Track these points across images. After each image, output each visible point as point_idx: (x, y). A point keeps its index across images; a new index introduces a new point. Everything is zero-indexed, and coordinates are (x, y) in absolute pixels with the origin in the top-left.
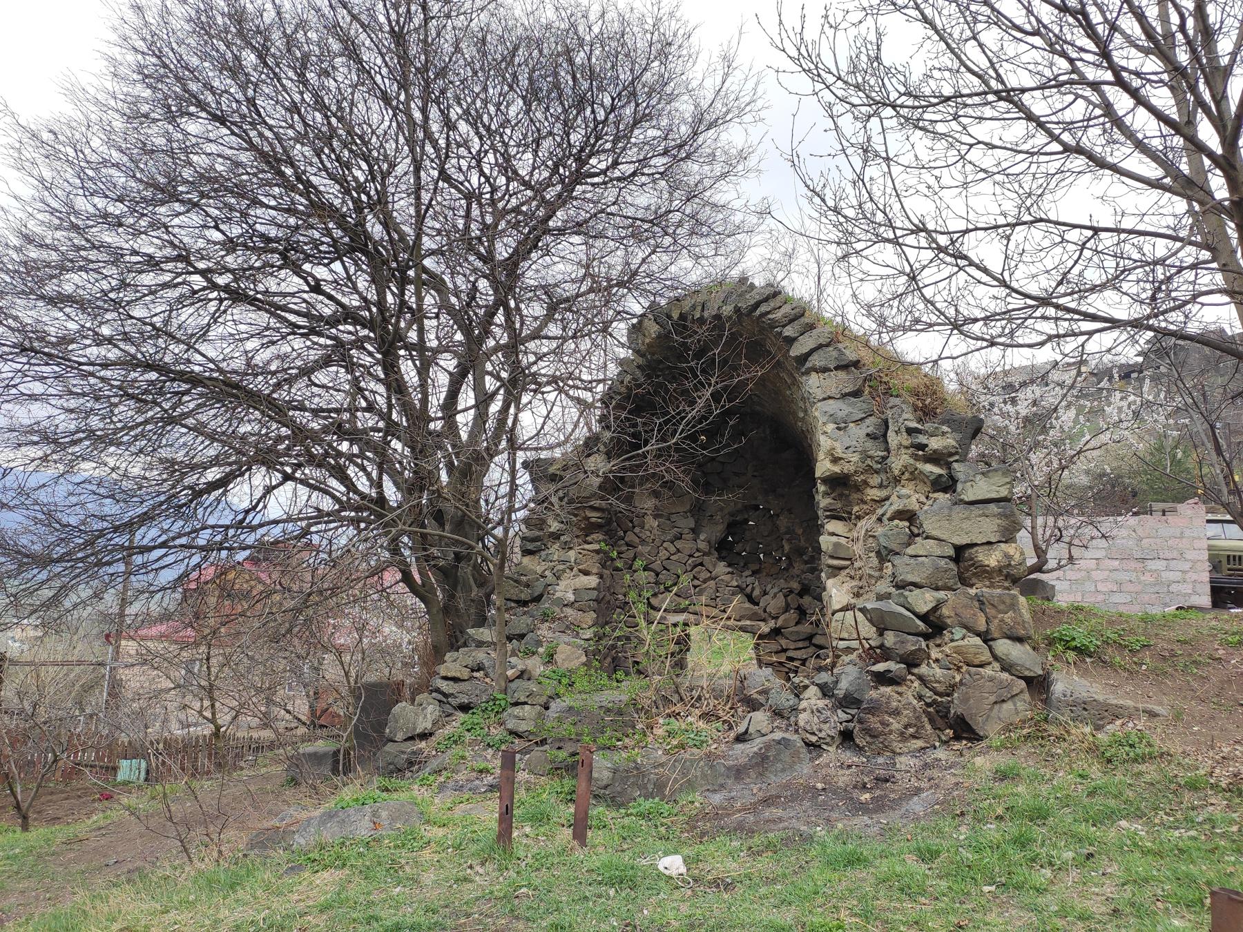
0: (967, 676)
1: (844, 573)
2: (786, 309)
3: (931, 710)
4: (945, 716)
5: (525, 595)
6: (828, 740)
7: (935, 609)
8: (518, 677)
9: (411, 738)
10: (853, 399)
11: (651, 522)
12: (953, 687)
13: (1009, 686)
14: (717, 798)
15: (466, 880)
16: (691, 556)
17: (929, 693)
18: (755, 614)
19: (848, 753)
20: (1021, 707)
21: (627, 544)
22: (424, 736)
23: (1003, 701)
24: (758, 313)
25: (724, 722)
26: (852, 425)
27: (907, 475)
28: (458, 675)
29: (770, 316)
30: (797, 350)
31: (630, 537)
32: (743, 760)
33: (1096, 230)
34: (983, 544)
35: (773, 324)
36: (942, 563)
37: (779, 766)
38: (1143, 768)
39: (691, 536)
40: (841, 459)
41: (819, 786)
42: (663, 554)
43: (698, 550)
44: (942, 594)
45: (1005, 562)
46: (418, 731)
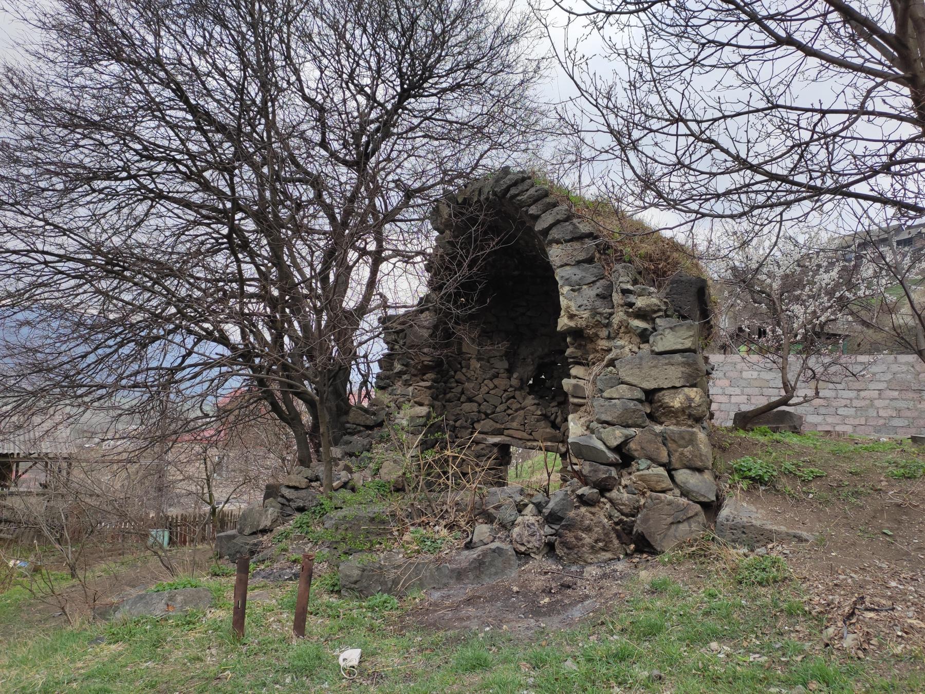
0: (649, 500)
1: (583, 409)
2: (532, 191)
3: (618, 527)
4: (631, 532)
5: (371, 420)
6: (535, 550)
7: (626, 442)
8: (341, 487)
9: (254, 533)
10: (586, 265)
11: (475, 364)
12: (638, 509)
13: (685, 509)
14: (436, 595)
15: (199, 659)
16: (505, 391)
17: (617, 514)
18: (555, 437)
19: (550, 561)
20: (693, 529)
21: (457, 382)
22: (264, 531)
23: (679, 522)
24: (508, 195)
25: (465, 531)
26: (585, 287)
27: (623, 329)
28: (297, 484)
29: (519, 198)
30: (540, 226)
31: (459, 376)
32: (464, 565)
33: (824, 113)
34: (669, 388)
35: (522, 204)
36: (631, 404)
37: (493, 570)
38: (763, 590)
39: (505, 375)
40: (575, 315)
41: (515, 589)
42: (484, 389)
43: (511, 386)
44: (631, 431)
45: (686, 404)
46: (261, 527)
